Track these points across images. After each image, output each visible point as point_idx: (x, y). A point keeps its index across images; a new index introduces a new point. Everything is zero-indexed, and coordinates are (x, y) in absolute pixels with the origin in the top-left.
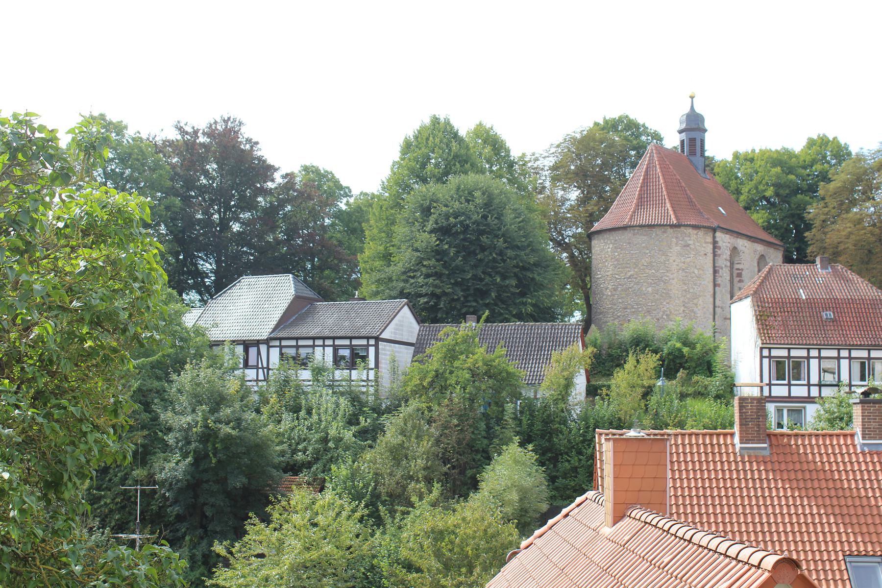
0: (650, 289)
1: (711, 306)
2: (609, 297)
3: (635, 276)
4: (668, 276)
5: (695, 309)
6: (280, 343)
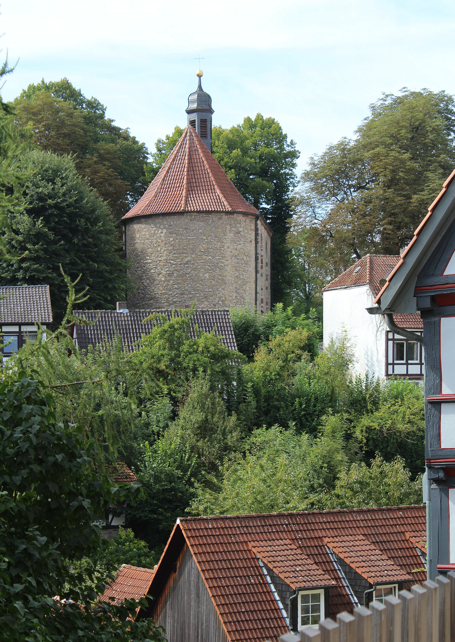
0: (207, 275)
1: (254, 292)
2: (162, 283)
3: (192, 262)
4: (223, 263)
5: (245, 295)
6: (20, 329)
